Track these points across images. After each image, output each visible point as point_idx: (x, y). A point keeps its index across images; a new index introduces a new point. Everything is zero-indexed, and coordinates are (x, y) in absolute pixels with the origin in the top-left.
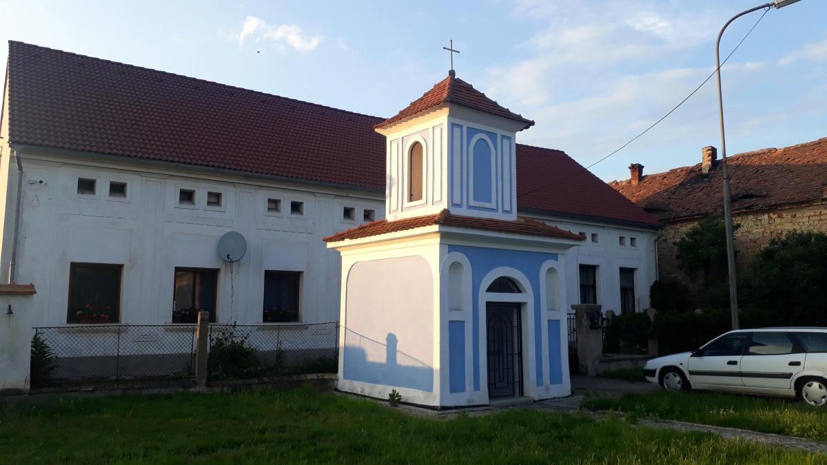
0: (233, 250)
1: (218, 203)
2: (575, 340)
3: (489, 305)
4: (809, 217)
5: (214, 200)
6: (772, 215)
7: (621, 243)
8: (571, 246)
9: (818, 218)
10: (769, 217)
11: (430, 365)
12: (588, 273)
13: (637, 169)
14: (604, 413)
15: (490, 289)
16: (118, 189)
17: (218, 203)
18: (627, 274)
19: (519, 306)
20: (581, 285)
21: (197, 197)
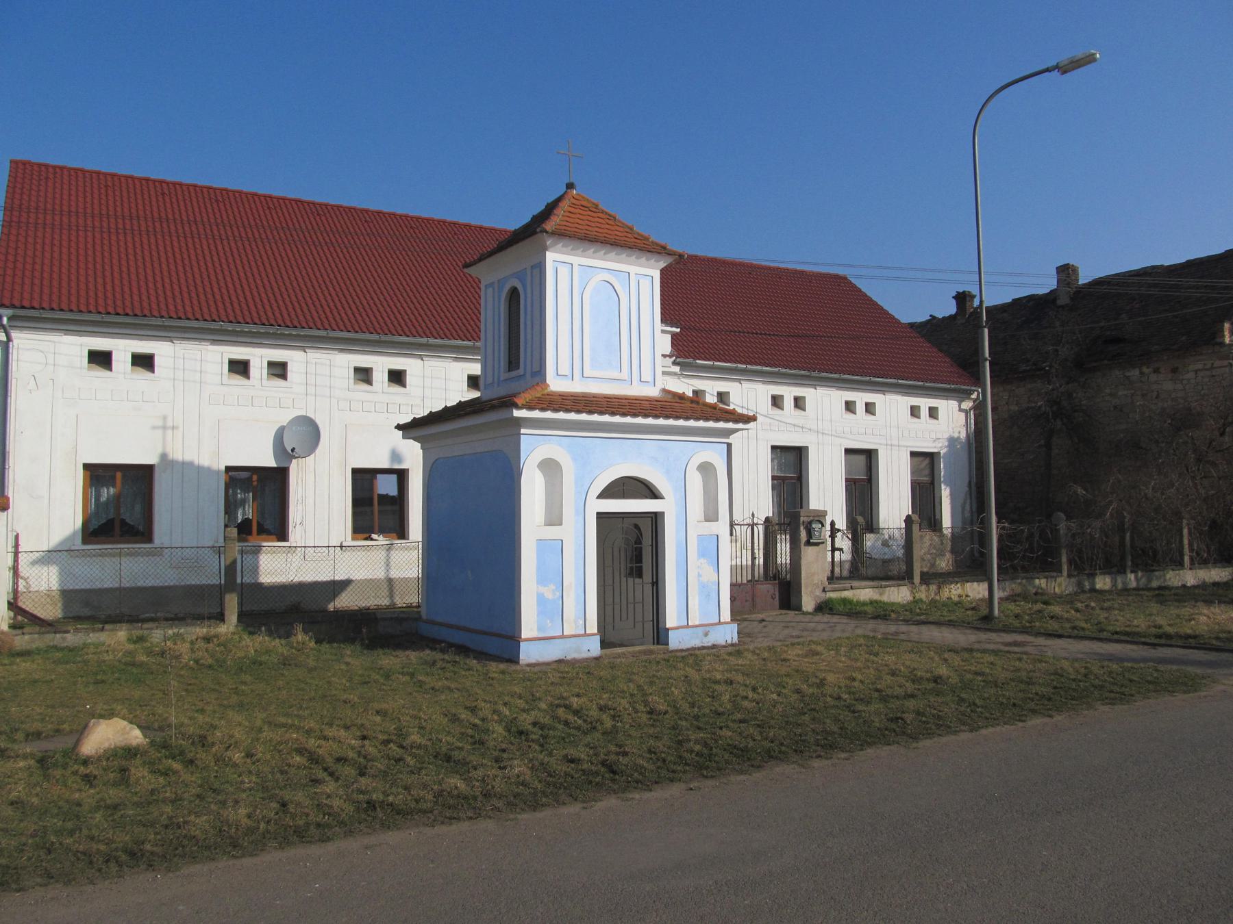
0: (306, 435)
1: (283, 376)
2: (750, 563)
3: (601, 516)
4: (1196, 371)
5: (278, 371)
6: (1145, 370)
7: (912, 414)
8: (735, 431)
9: (1208, 373)
10: (1142, 373)
11: (57, 595)
12: (791, 466)
13: (1066, 272)
14: (102, 629)
15: (600, 496)
16: (144, 362)
17: (283, 376)
18: (925, 461)
19: (656, 519)
20: (847, 480)
21: (254, 370)
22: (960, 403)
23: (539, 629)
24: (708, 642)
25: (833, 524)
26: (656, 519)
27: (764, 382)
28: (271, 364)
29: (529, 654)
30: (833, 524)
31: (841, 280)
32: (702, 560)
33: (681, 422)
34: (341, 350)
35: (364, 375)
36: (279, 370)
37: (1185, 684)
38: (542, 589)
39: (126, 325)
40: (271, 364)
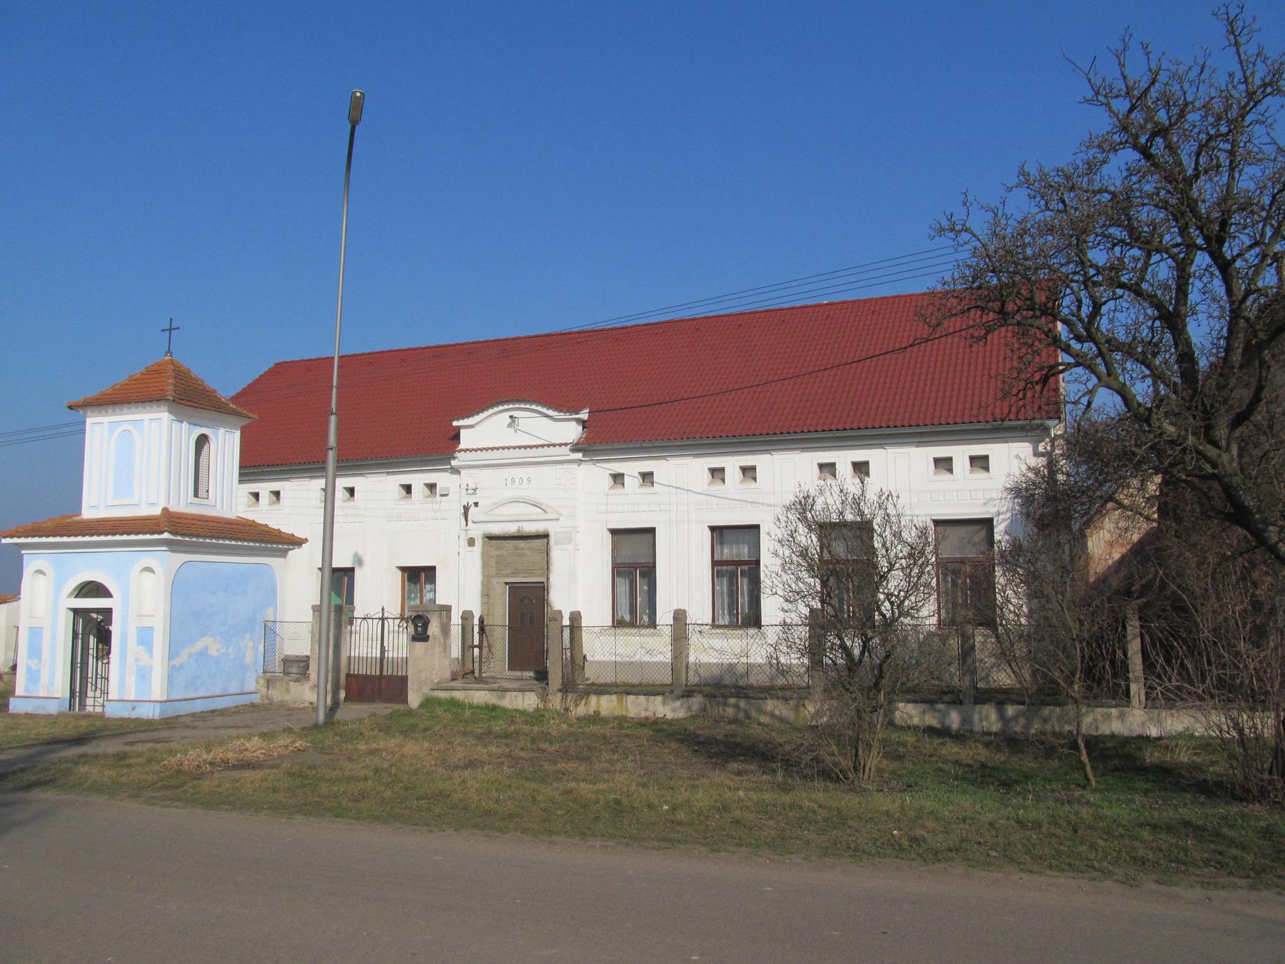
3: (76, 612)
19: (108, 612)
22: (1035, 444)
23: (26, 690)
24: (134, 715)
25: (680, 616)
26: (108, 612)
27: (696, 456)
28: (973, 459)
29: (15, 706)
30: (680, 616)
31: (280, 369)
32: (141, 648)
33: (110, 538)
34: (311, 477)
35: (828, 469)
36: (749, 472)
37: (230, 804)
38: (30, 662)
39: (733, 444)
40: (973, 459)
